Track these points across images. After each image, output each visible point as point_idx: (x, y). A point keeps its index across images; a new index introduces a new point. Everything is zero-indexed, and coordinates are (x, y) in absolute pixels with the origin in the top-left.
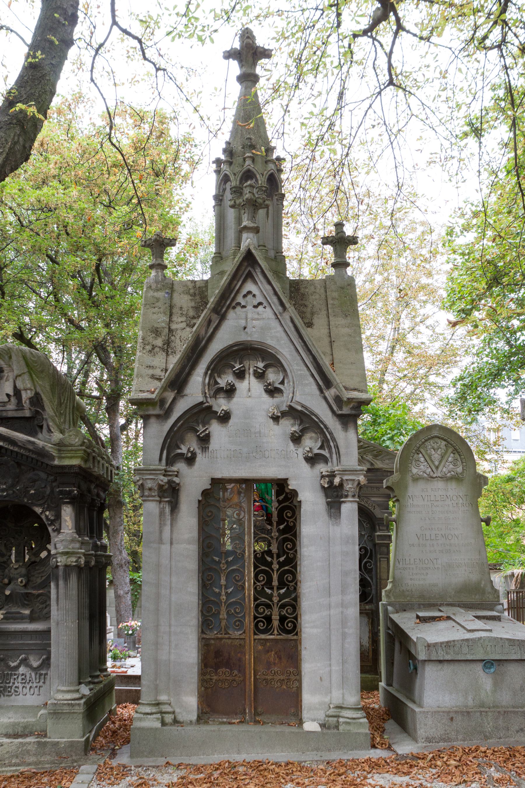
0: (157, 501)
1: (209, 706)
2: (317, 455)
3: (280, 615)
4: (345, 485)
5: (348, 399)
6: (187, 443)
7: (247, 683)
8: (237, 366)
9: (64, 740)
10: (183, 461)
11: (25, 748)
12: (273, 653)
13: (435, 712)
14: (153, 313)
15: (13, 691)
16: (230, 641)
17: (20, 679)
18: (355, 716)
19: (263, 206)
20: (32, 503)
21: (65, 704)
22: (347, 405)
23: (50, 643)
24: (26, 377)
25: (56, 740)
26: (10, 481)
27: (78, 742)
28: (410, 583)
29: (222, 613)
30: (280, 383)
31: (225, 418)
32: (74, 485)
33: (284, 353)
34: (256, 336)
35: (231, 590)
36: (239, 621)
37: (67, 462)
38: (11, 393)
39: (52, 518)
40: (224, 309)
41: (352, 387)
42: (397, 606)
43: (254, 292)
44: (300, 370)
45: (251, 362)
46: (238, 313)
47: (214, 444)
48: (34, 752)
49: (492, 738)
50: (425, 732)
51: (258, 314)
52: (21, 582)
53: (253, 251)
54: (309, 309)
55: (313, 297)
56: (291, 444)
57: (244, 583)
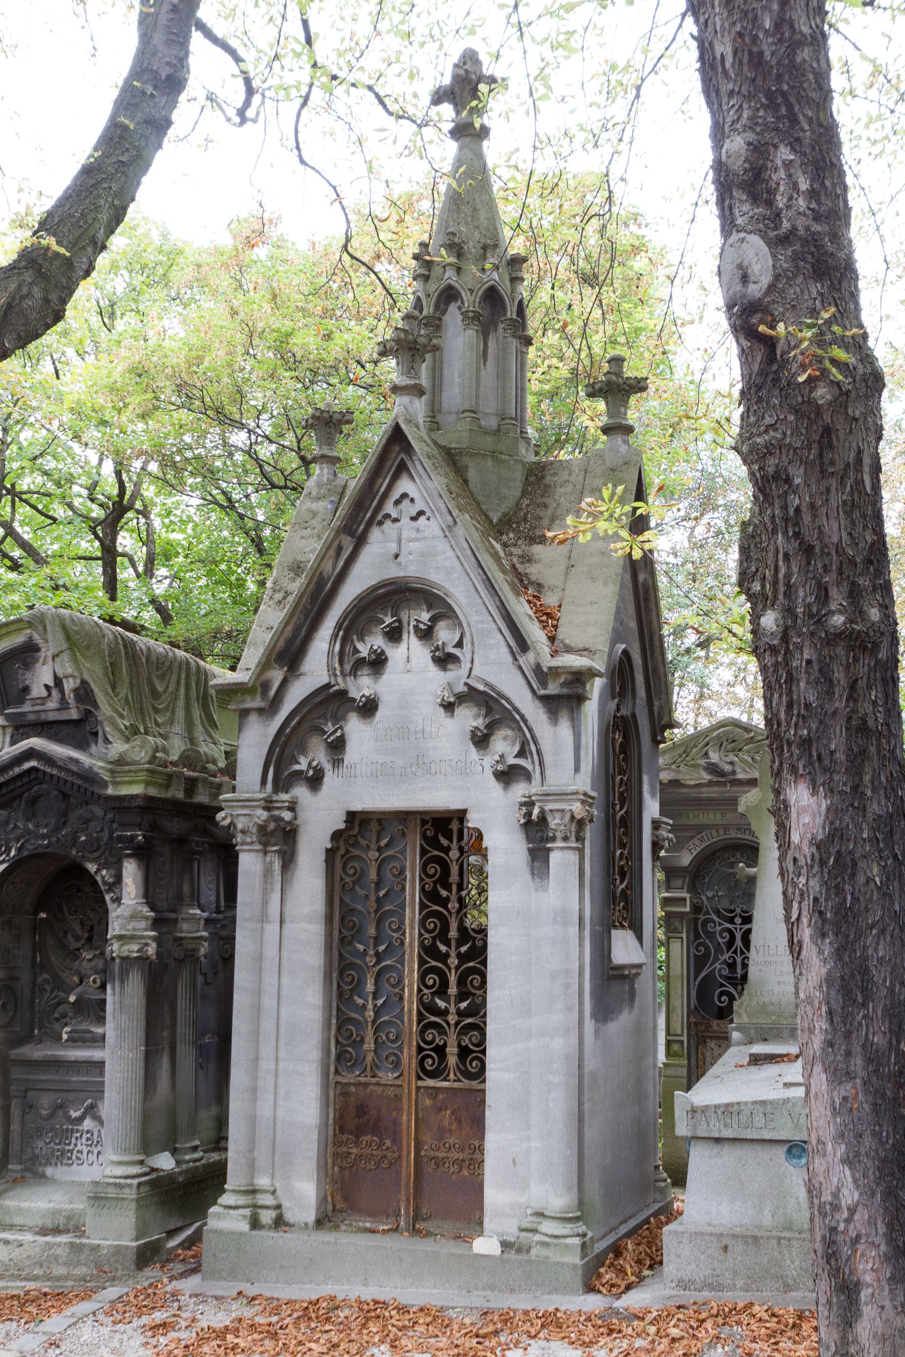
0: (258, 851)
1: (345, 1199)
2: (512, 767)
3: (459, 1046)
4: (549, 819)
5: (550, 668)
6: (311, 754)
7: (404, 1163)
8: (389, 620)
9: (108, 1243)
10: (304, 783)
11: (52, 1251)
12: (448, 1112)
13: (696, 1234)
14: (303, 538)
15: (74, 1157)
16: (381, 1088)
17: (85, 1136)
18: (556, 1232)
19: (429, 348)
20: (83, 857)
21: (110, 1184)
22: (555, 679)
23: (103, 1082)
24: (65, 657)
25: (97, 1242)
26: (53, 821)
27: (127, 1247)
28: (777, 989)
29: (367, 1039)
30: (456, 646)
31: (369, 708)
32: (139, 826)
33: (457, 594)
34: (413, 568)
35: (381, 1001)
36: (395, 1055)
37: (125, 791)
38: (51, 684)
39: (111, 880)
40: (362, 527)
41: (580, 646)
42: (752, 1031)
43: (411, 495)
44: (481, 622)
45: (412, 612)
46: (387, 531)
47: (351, 754)
48: (64, 1259)
49: (798, 1289)
50: (678, 1270)
51: (418, 530)
52: (94, 981)
53: (403, 426)
54: (549, 512)
55: (563, 490)
56: (473, 749)
57: (403, 990)
